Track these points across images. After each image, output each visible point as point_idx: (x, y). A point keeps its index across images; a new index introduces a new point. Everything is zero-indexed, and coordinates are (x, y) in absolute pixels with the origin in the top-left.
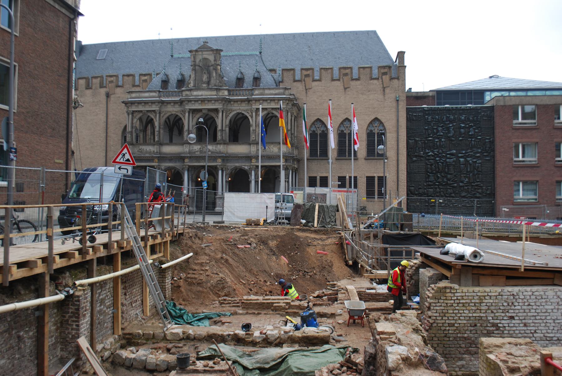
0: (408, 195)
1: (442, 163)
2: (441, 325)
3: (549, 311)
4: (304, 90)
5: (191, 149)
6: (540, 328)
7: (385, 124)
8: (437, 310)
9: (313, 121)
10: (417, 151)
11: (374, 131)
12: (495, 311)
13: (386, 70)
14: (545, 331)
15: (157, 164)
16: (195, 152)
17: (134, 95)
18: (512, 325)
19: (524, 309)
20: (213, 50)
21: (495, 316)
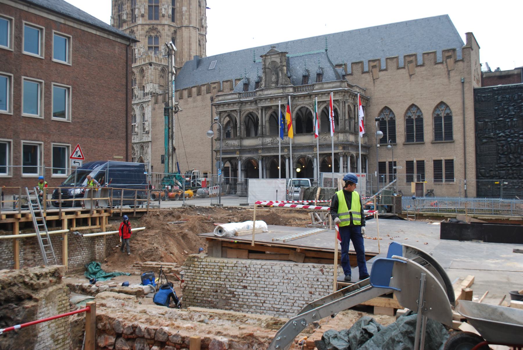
0: (477, 177)
1: (515, 144)
2: (191, 288)
3: (276, 284)
4: (372, 81)
5: (264, 141)
6: (268, 299)
7: (450, 107)
8: (188, 275)
9: (381, 109)
10: (487, 133)
11: (440, 115)
12: (232, 280)
13: (450, 54)
14: (273, 302)
17: (220, 98)
19: (255, 281)
20: (278, 53)
21: (232, 285)
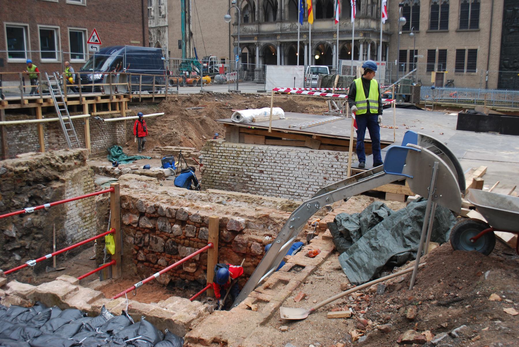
0: (500, 68)
2: (210, 172)
6: (284, 183)
12: (249, 165)
15: (256, 41)
16: (286, 30)
18: (262, 178)
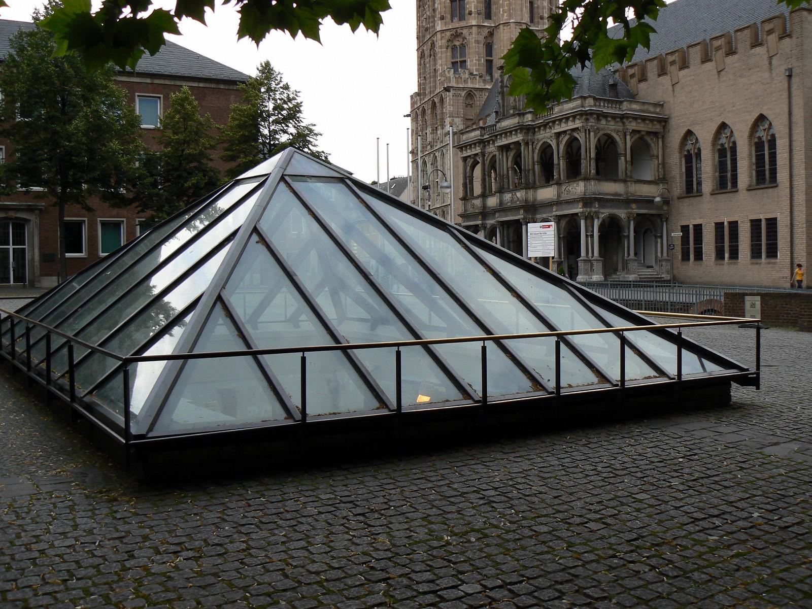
12: (508, 466)
